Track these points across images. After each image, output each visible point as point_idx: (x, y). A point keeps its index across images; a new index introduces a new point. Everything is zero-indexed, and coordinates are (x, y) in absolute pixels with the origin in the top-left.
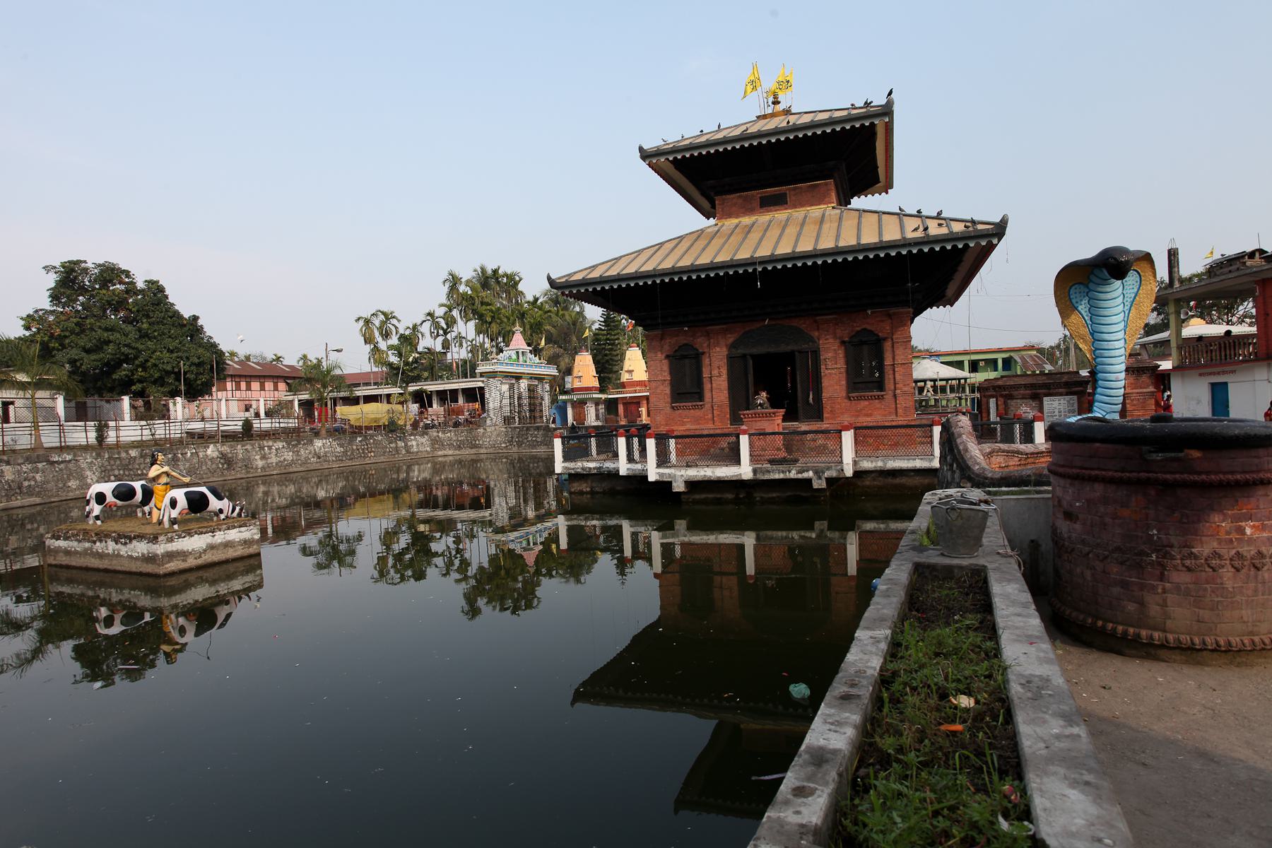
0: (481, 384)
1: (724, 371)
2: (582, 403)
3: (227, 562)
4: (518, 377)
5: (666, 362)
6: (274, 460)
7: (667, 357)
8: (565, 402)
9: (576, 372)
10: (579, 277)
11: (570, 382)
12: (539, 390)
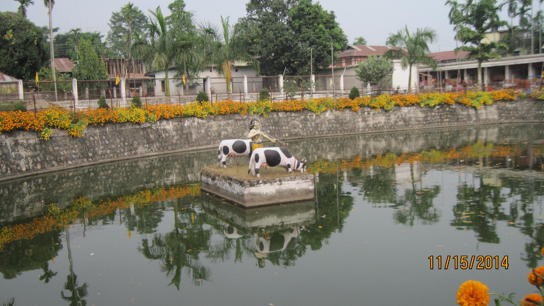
3: (294, 202)
6: (371, 122)
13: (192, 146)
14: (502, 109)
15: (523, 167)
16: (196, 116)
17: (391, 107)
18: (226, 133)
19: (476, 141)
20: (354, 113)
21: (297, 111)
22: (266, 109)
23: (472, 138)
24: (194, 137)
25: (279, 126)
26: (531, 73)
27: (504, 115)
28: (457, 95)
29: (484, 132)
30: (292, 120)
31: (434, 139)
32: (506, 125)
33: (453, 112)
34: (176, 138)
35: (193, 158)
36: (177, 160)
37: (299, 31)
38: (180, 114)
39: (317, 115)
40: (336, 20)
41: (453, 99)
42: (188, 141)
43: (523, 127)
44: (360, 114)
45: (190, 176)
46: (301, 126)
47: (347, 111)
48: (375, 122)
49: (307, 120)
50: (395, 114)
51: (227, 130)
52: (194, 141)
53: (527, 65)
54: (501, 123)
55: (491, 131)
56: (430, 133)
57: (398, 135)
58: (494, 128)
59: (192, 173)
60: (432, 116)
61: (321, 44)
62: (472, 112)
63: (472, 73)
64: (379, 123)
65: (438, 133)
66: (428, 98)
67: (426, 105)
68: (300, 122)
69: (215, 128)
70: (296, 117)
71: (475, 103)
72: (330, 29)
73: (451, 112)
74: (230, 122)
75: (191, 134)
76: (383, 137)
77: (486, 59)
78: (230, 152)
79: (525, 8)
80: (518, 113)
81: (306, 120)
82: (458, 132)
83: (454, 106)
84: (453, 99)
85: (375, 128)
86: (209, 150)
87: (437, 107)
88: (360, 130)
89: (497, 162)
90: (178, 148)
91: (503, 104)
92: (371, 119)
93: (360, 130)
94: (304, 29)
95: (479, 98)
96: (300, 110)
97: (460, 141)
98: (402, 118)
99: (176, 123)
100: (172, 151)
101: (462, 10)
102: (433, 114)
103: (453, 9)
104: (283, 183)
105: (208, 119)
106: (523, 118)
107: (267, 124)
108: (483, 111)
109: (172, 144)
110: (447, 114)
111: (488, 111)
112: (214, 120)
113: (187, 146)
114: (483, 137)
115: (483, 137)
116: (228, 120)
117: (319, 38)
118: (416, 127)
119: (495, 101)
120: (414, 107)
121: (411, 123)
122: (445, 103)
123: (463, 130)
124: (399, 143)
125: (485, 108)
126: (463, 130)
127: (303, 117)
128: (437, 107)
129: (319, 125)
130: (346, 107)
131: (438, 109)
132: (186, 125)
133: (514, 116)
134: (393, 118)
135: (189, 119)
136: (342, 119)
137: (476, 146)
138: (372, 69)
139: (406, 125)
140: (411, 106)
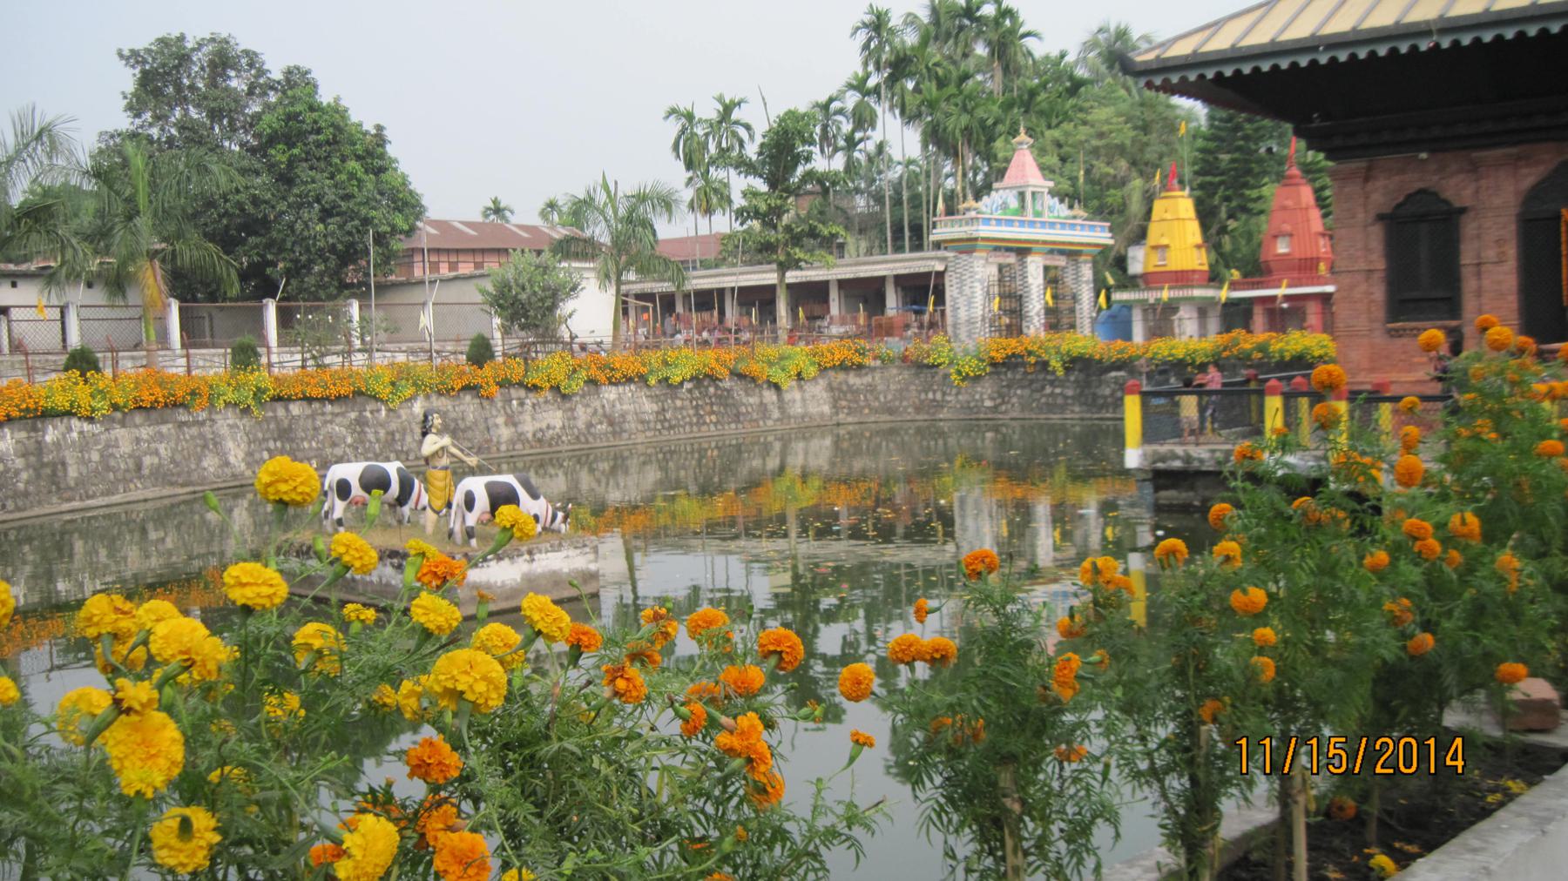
0: (939, 267)
1: (1511, 251)
2: (1171, 308)
4: (1022, 251)
5: (1376, 235)
6: (529, 427)
7: (1381, 217)
8: (1128, 306)
9: (1155, 234)
10: (1183, 49)
11: (1138, 260)
12: (1069, 279)
13: (69, 500)
14: (840, 390)
15: (886, 534)
16: (74, 415)
17: (577, 386)
18: (156, 460)
19: (781, 470)
20: (485, 403)
21: (339, 399)
22: (259, 392)
23: (773, 463)
24: (72, 472)
25: (292, 440)
26: (892, 300)
27: (844, 403)
28: (733, 355)
29: (799, 446)
30: (325, 422)
31: (684, 468)
32: (851, 428)
33: (725, 398)
34: (24, 476)
35: (71, 533)
36: (29, 540)
37: (286, 179)
38: (32, 406)
39: (389, 410)
40: (391, 150)
41: (724, 364)
42: (57, 484)
43: (892, 432)
44: (500, 405)
45: (61, 586)
46: (349, 440)
47: (468, 398)
48: (538, 425)
49: (366, 423)
50: (587, 406)
51: (156, 453)
52: (72, 483)
53: (882, 279)
54: (838, 425)
55: (815, 444)
56: (672, 452)
57: (596, 460)
58: (823, 437)
59: (68, 575)
60: (675, 408)
61: (353, 215)
62: (770, 396)
63: (759, 300)
64: (548, 427)
65: (692, 452)
66: (665, 363)
67: (660, 381)
68: (348, 427)
69: (125, 448)
70: (337, 415)
71: (777, 375)
72: (376, 174)
73: (720, 397)
74: (164, 429)
75: (64, 464)
76: (561, 466)
77: (795, 264)
78: (353, 493)
79: (858, 135)
80: (877, 399)
81: (361, 422)
82: (739, 449)
83: (727, 384)
84: (724, 364)
85: (540, 441)
86: (114, 510)
87: (688, 385)
88: (503, 448)
89: (821, 524)
90: (32, 507)
91: (841, 376)
92: (527, 418)
93: (503, 448)
94: (303, 172)
95: (786, 363)
96: (346, 397)
97: (743, 471)
98: (605, 415)
99: (23, 435)
100: (18, 515)
101: (707, 135)
102: (679, 403)
103: (683, 132)
104: (536, 557)
105: (108, 421)
106: (891, 411)
107: (260, 435)
108: (797, 395)
109: (16, 495)
110: (712, 404)
111: (807, 395)
112: (123, 425)
113: (55, 500)
114: (796, 461)
115: (796, 461)
116: (158, 423)
117: (347, 197)
118: (640, 438)
119: (823, 370)
120: (633, 387)
121: (627, 426)
122: (706, 376)
123: (753, 444)
124: (599, 482)
125: (800, 388)
126: (753, 444)
127: (353, 415)
128: (688, 385)
129: (397, 436)
130: (467, 388)
131: (690, 391)
132: (48, 438)
133: (869, 406)
134: (582, 414)
135: (57, 421)
136: (455, 420)
137: (783, 483)
138: (527, 286)
139: (614, 433)
140: (623, 384)
